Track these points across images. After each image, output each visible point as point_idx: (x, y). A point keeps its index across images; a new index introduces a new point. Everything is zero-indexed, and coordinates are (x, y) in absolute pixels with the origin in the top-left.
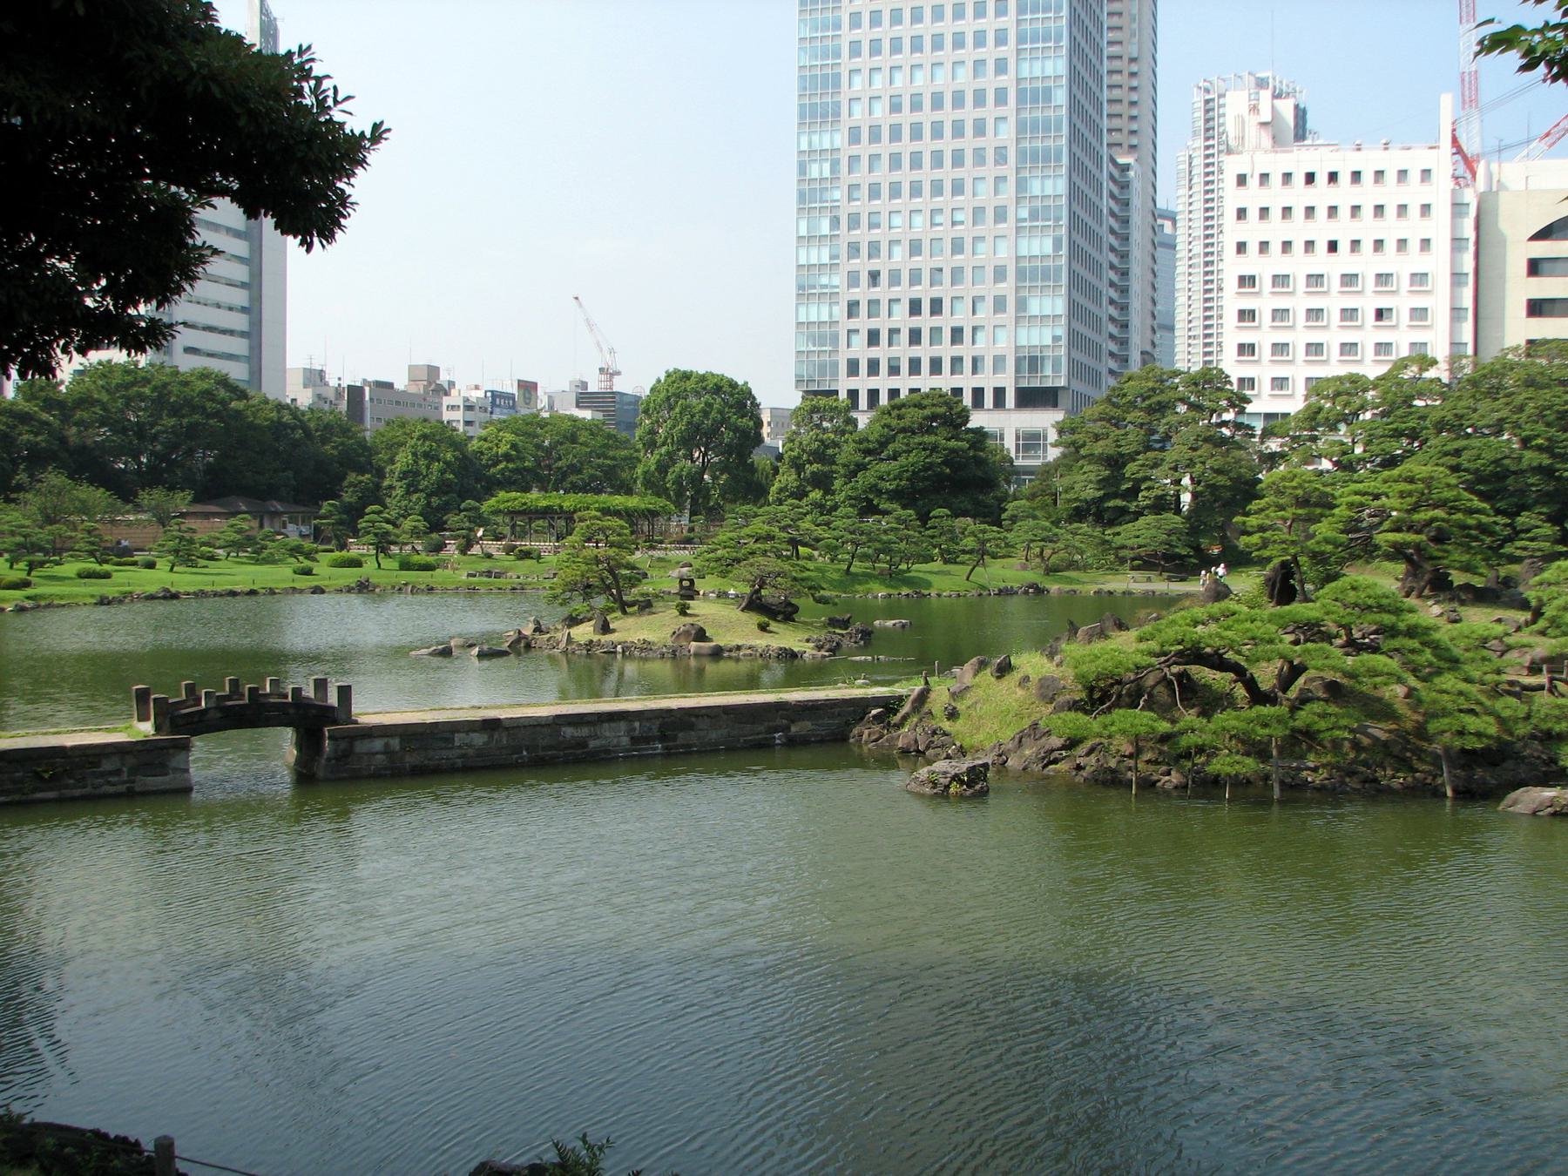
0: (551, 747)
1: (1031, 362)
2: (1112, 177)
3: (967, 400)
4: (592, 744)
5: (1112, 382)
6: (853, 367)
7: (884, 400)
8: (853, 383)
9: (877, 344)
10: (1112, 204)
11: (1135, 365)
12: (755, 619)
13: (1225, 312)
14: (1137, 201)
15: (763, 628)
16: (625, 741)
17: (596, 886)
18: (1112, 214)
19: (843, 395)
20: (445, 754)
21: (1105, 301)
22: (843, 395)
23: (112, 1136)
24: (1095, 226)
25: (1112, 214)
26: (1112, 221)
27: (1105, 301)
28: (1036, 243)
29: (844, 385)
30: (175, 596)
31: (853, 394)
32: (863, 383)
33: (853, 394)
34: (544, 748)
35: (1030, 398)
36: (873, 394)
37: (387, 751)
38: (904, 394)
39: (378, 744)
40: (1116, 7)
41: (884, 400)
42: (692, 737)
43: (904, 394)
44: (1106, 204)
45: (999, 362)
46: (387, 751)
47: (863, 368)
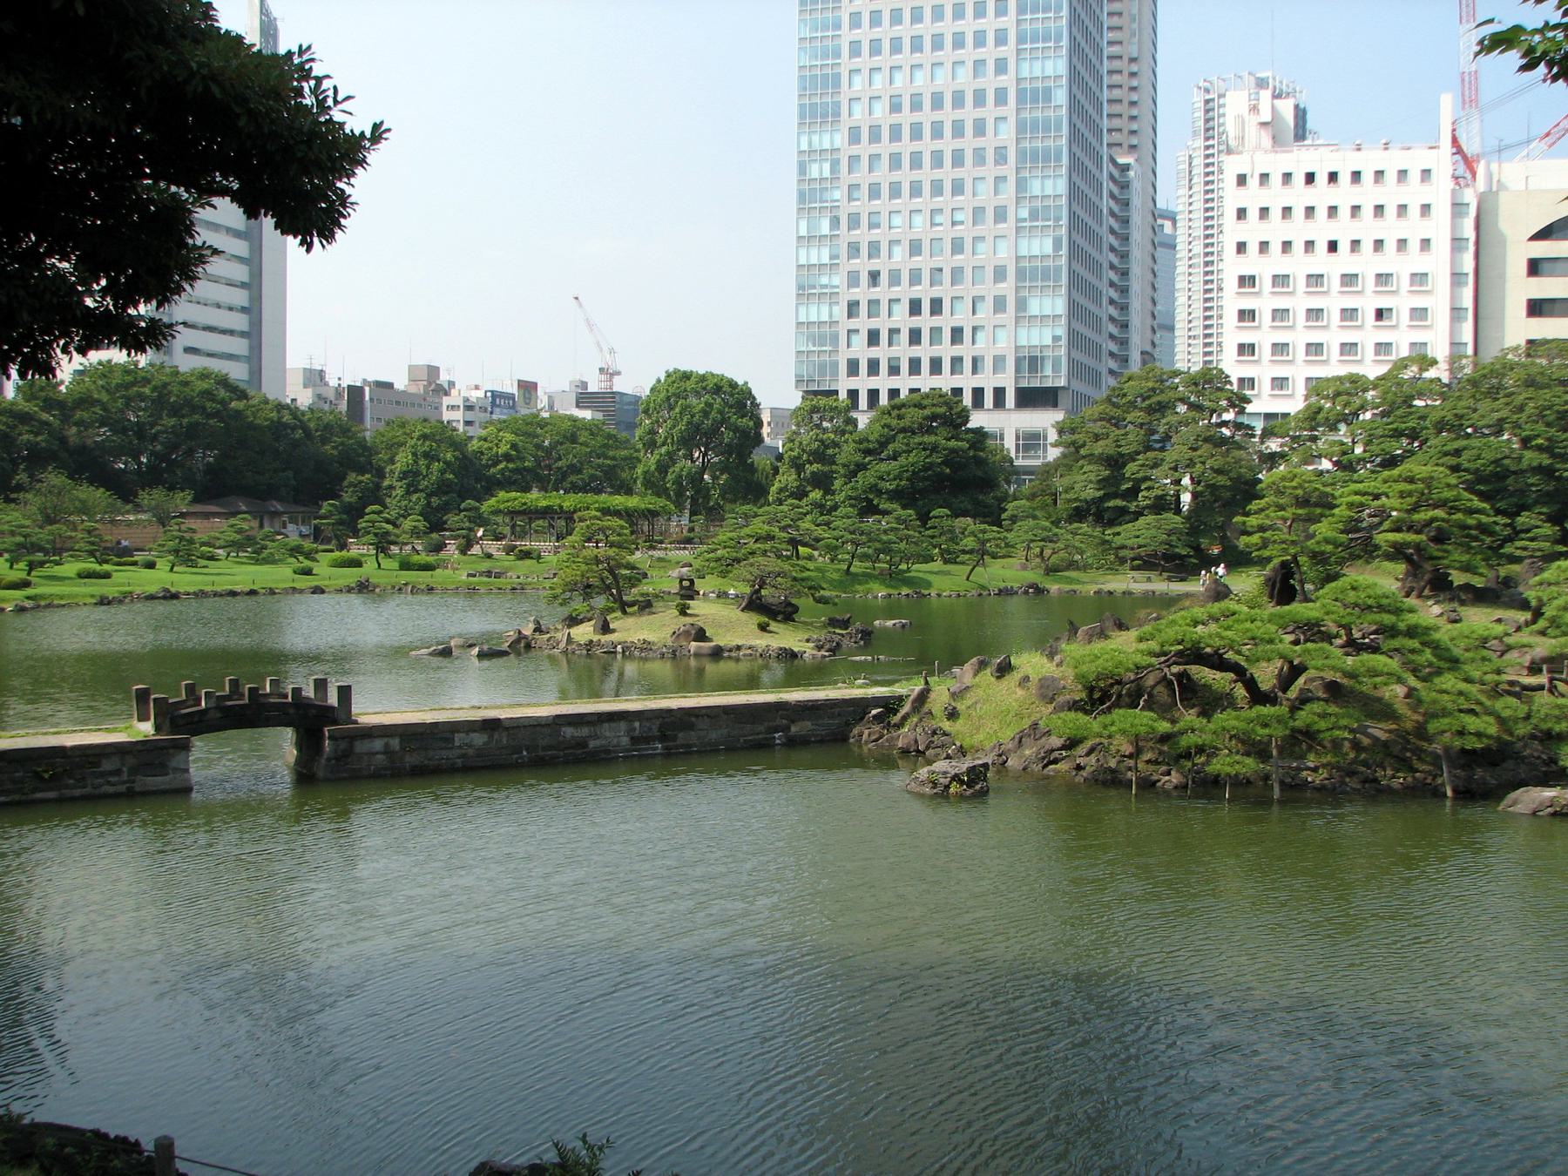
0: (551, 747)
1: (1031, 362)
2: (1112, 177)
3: (967, 400)
4: (592, 744)
5: (1112, 382)
6: (853, 367)
7: (884, 400)
8: (853, 383)
9: (877, 344)
10: (1112, 204)
11: (1135, 365)
12: (755, 619)
13: (1225, 312)
14: (1137, 201)
15: (763, 628)
16: (625, 741)
17: (596, 886)
18: (1112, 214)
19: (843, 395)
20: (445, 754)
21: (1105, 301)
22: (843, 395)
23: (112, 1136)
24: (1095, 226)
25: (1112, 214)
26: (1112, 221)
27: (1105, 301)
28: (1036, 243)
29: (844, 385)
30: (175, 596)
31: (853, 394)
32: (863, 383)
33: (853, 394)
34: (544, 748)
35: (1030, 398)
36: (873, 394)
37: (387, 751)
38: (904, 394)
39: (378, 744)
40: (1116, 7)
41: (884, 400)
42: (692, 737)
43: (904, 394)
44: (1106, 204)
45: (999, 362)
46: (387, 751)
47: (863, 368)
